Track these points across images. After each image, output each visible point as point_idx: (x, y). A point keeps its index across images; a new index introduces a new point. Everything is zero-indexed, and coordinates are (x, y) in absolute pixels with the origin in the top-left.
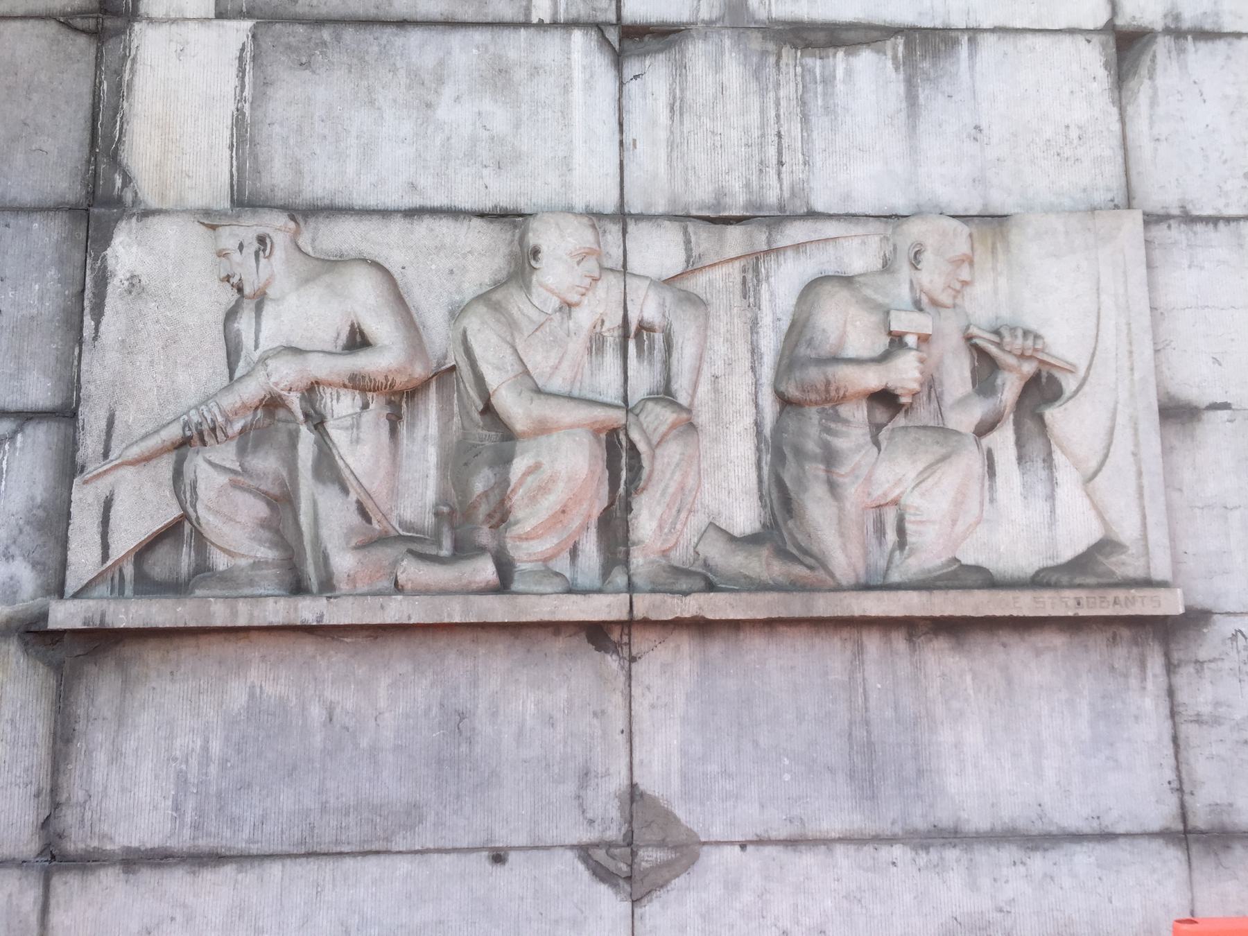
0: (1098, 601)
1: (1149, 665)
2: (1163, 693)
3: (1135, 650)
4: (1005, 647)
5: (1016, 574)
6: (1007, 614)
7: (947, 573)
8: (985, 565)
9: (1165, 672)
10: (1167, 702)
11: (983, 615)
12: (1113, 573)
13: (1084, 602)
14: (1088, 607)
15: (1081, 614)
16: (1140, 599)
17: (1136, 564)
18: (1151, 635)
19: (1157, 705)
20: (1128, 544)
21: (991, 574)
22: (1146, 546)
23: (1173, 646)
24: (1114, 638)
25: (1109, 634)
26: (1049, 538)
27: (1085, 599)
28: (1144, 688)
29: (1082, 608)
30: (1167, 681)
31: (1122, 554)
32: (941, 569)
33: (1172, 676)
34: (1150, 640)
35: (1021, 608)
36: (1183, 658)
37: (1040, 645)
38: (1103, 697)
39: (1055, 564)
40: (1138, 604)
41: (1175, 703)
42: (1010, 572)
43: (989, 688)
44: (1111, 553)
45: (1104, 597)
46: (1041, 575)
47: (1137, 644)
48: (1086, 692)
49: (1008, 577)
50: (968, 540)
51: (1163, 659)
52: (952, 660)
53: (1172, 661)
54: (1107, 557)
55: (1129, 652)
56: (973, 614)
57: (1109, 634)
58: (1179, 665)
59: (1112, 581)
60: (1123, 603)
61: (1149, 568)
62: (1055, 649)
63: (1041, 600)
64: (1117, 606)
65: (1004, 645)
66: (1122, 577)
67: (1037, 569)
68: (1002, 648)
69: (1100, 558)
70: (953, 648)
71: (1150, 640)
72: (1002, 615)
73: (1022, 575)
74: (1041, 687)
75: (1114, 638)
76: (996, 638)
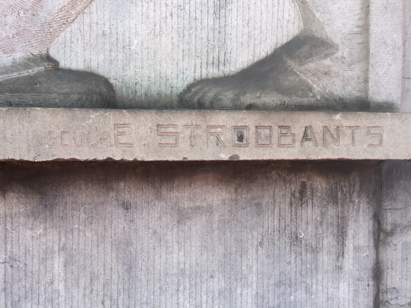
0: (276, 132)
1: (350, 233)
2: (367, 275)
3: (332, 211)
4: (127, 209)
5: (154, 90)
6: (101, 157)
7: (18, 79)
8: (102, 71)
9: (372, 244)
10: (371, 288)
11: (50, 159)
12: (310, 89)
13: (250, 135)
14: (259, 145)
15: (242, 158)
16: (349, 132)
17: (345, 74)
18: (357, 188)
19: (356, 292)
20: (337, 40)
21: (114, 91)
22: (366, 45)
23: (387, 204)
24: (302, 193)
25: (295, 187)
26: (214, 30)
27: (253, 129)
28: (340, 268)
29: (247, 145)
30: (373, 256)
31: (326, 56)
32: (6, 73)
33: (381, 249)
34: (355, 195)
35: (130, 145)
36: (399, 221)
37: (186, 204)
38: (279, 284)
39: (221, 74)
40: (345, 141)
41: (382, 287)
42: (145, 83)
43: (93, 278)
44: (309, 56)
45: (288, 127)
46: (193, 90)
47: (336, 202)
48: (252, 278)
49: (141, 92)
50: (74, 26)
51: (371, 222)
52: (29, 232)
53: (385, 227)
54: (301, 63)
55: (323, 214)
56: (29, 157)
57: (295, 187)
58: (392, 233)
59: (305, 101)
60: (319, 137)
61: (366, 81)
62: (210, 210)
63: (171, 130)
64: (307, 144)
65: (126, 207)
66: (322, 97)
67: (190, 80)
68: (121, 211)
69: (291, 64)
70: (34, 215)
71: (355, 195)
72: (91, 158)
73: (166, 91)
74: (182, 272)
75: (302, 193)
76: (112, 194)
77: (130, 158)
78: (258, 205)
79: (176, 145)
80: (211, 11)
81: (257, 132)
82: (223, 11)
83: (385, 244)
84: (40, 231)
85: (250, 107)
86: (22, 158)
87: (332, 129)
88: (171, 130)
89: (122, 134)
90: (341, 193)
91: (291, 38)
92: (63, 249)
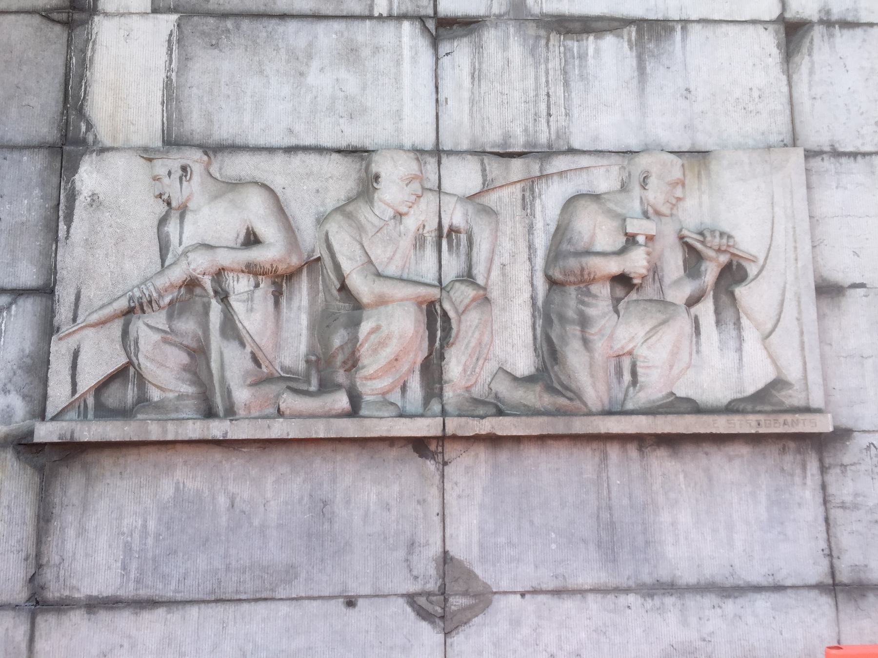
0: (772, 422)
1: (808, 468)
2: (818, 488)
3: (799, 457)
5: (715, 404)
6: (708, 432)
7: (666, 403)
9: (819, 472)
10: (821, 494)
11: (691, 432)
12: (783, 403)
13: (762, 423)
15: (760, 432)
16: (802, 421)
17: (799, 396)
18: (810, 446)
22: (806, 384)
23: (825, 454)
24: (784, 448)
25: (780, 446)
27: (763, 421)
28: (805, 484)
29: (762, 427)
31: (789, 389)
33: (825, 475)
34: (809, 450)
35: (718, 427)
36: (832, 462)
37: (732, 453)
38: (776, 490)
39: (742, 397)
40: (801, 425)
41: (827, 494)
42: (711, 402)
43: (696, 484)
44: (782, 389)
45: (777, 420)
46: (733, 404)
48: (764, 487)
51: (818, 463)
52: (669, 464)
53: (825, 464)
55: (794, 459)
57: (780, 446)
58: (829, 468)
59: (782, 408)
60: (790, 424)
61: (808, 399)
62: (742, 456)
63: (732, 422)
65: (707, 454)
67: (729, 400)
68: (705, 456)
69: (774, 392)
70: (670, 456)
71: (809, 450)
73: (719, 404)
75: (784, 448)
77: (718, 432)
78: (764, 454)
79: (734, 427)
80: (736, 370)
81: (765, 423)
82: (741, 370)
83: (826, 473)
84: (674, 463)
85: (760, 412)
86: (494, 431)
87: (795, 420)
88: (732, 422)
89: (715, 423)
90: (685, 477)
91: (771, 380)
92: (683, 471)
